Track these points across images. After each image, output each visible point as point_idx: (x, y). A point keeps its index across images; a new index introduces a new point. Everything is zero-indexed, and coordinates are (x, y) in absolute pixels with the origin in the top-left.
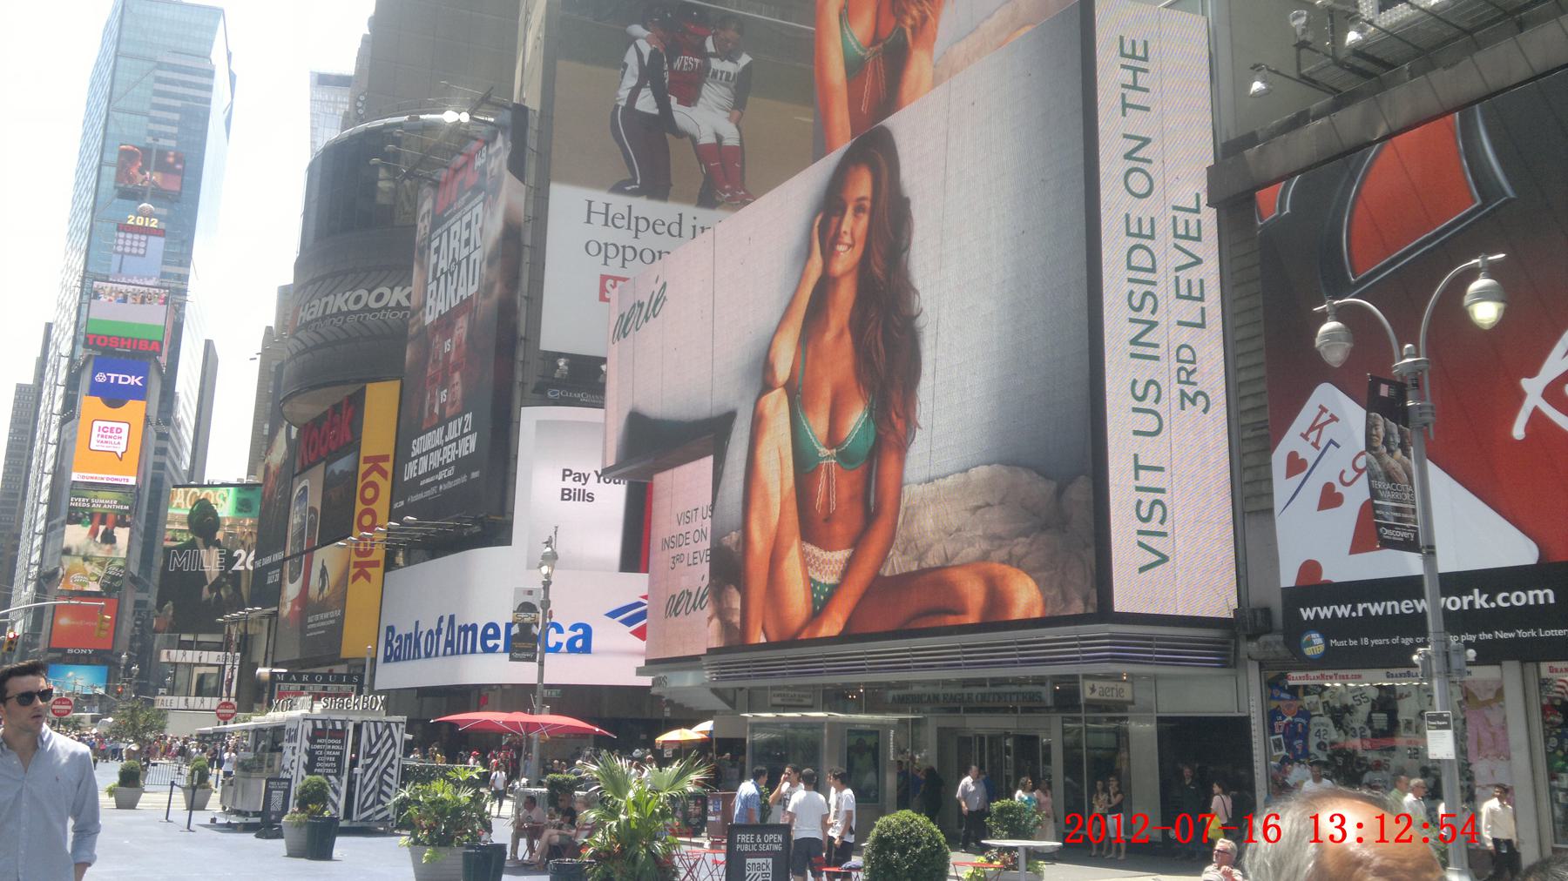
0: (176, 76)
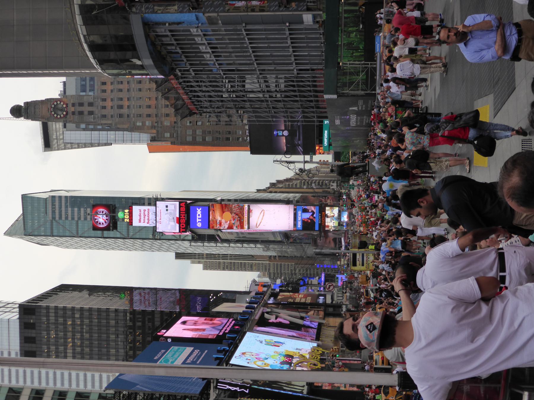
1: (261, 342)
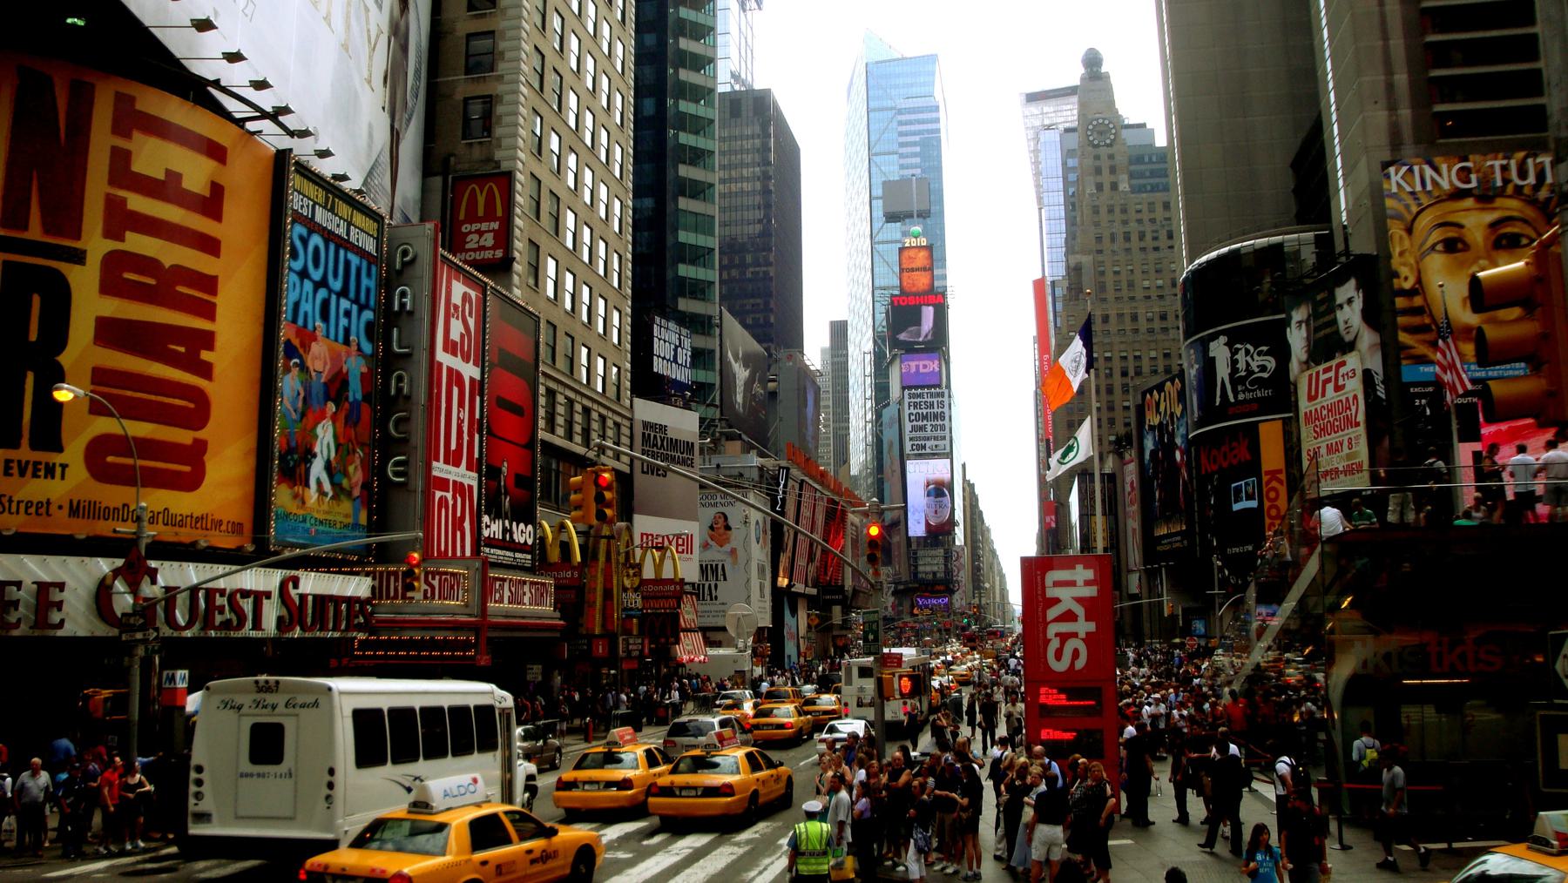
0: (913, 117)
1: (733, 552)
